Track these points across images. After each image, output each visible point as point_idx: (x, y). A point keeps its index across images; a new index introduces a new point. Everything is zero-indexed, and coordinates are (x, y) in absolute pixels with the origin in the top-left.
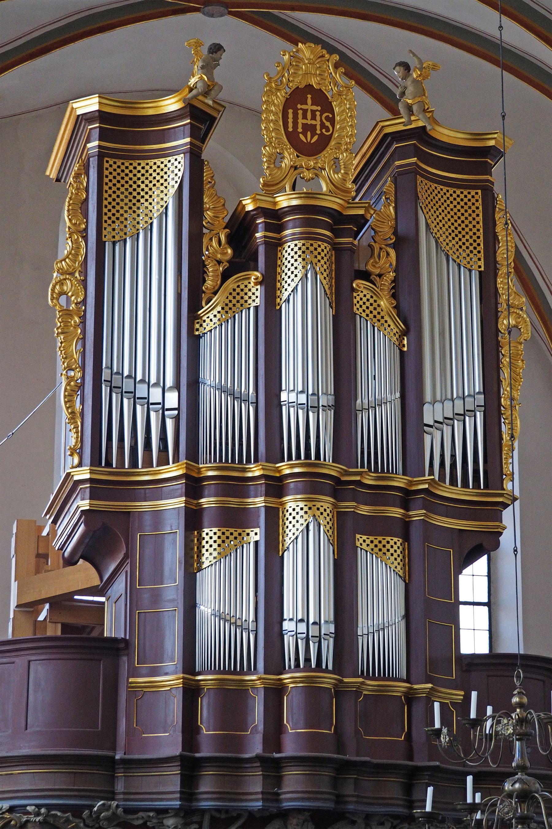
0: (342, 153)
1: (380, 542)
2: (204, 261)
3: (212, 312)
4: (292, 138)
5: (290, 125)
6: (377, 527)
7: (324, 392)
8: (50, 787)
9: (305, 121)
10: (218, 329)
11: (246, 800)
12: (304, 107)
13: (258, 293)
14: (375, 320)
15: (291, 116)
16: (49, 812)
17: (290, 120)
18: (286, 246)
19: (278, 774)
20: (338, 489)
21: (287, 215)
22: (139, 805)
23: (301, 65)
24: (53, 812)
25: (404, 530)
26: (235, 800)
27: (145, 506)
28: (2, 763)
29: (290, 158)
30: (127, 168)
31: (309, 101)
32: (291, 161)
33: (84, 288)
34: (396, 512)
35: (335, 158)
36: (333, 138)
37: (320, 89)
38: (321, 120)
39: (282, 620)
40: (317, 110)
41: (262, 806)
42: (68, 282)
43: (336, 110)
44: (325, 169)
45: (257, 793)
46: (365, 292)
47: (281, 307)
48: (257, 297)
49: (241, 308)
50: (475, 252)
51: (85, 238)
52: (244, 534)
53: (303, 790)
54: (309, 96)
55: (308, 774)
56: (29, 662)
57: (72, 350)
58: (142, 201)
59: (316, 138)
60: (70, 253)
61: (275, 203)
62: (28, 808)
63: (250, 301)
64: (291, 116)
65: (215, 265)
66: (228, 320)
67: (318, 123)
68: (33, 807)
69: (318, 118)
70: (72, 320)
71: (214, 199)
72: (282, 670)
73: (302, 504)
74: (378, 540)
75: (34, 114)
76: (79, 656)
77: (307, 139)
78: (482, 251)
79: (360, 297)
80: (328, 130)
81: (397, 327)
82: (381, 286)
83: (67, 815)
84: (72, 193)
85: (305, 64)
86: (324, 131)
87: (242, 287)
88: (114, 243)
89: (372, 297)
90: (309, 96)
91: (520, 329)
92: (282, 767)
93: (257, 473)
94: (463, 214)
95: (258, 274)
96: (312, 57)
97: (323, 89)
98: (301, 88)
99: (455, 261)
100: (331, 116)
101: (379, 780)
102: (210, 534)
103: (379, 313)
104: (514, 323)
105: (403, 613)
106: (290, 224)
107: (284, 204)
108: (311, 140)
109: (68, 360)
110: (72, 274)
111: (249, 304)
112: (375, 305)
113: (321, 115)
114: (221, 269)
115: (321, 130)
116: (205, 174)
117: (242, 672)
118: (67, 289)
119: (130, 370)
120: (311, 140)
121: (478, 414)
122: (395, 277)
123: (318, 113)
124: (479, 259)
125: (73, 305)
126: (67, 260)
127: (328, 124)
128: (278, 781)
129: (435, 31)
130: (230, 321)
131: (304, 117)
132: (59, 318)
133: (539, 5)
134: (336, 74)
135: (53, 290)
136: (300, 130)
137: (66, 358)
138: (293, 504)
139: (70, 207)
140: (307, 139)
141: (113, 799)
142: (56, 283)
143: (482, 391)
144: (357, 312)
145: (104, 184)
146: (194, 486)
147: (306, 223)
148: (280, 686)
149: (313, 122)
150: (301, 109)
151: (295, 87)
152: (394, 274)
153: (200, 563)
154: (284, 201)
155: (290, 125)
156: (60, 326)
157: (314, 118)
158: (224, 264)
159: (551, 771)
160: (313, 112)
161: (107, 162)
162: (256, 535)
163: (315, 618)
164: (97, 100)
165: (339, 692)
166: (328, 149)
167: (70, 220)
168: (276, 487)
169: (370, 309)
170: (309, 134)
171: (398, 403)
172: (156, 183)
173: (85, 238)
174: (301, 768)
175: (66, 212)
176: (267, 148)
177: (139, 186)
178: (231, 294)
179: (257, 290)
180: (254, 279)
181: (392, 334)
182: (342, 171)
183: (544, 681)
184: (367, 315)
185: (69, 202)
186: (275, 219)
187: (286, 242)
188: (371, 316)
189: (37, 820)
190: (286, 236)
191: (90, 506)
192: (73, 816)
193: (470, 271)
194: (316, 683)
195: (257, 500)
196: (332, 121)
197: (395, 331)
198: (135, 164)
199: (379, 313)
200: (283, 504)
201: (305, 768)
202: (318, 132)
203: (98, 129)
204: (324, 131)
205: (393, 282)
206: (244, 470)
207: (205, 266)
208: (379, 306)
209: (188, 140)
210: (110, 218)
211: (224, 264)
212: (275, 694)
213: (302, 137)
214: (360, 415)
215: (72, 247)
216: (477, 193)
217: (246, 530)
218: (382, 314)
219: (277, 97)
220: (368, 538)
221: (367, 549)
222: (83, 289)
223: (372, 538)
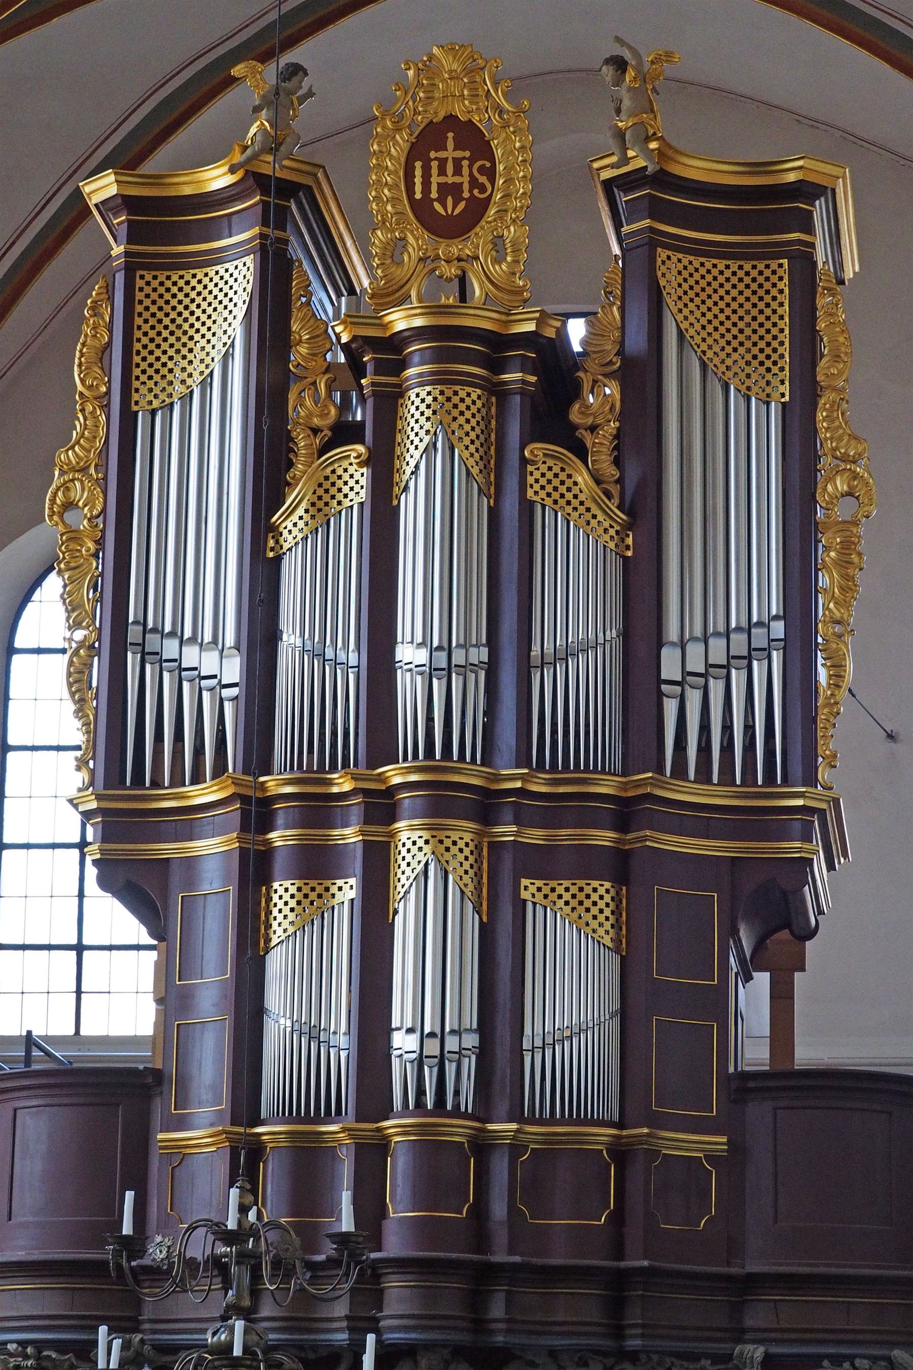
0: (508, 227)
1: (581, 889)
2: (290, 431)
3: (290, 520)
4: (422, 211)
5: (418, 188)
7: (462, 641)
8: (53, 1313)
9: (442, 179)
10: (300, 545)
11: (328, 1331)
12: (442, 154)
13: (363, 481)
14: (569, 509)
15: (418, 172)
16: (40, 1352)
17: (418, 180)
18: (412, 394)
19: (376, 1287)
20: (485, 806)
21: (409, 343)
22: (173, 1340)
23: (437, 81)
24: (45, 1353)
25: (620, 867)
26: (309, 1331)
27: (168, 849)
28: (2, 1272)
29: (418, 244)
30: (175, 284)
31: (450, 144)
32: (419, 250)
33: (102, 491)
34: (604, 837)
35: (495, 237)
36: (492, 201)
37: (470, 121)
38: (471, 175)
39: (388, 1031)
40: (464, 158)
41: (349, 1339)
42: (77, 484)
43: (499, 153)
44: (477, 258)
45: (339, 1319)
46: (550, 462)
47: (399, 502)
48: (362, 487)
49: (339, 508)
50: (775, 370)
51: (106, 408)
52: (334, 889)
53: (412, 1312)
54: (450, 135)
55: (422, 1287)
56: (15, 1110)
57: (83, 596)
58: (197, 337)
59: (462, 205)
60: (82, 436)
61: (385, 327)
62: (9, 1346)
63: (352, 495)
64: (418, 172)
65: (309, 436)
66: (317, 529)
67: (465, 180)
68: (15, 1346)
69: (465, 171)
70: (82, 546)
71: (309, 325)
72: (387, 1112)
74: (564, 886)
75: (336, 139)
76: (65, 1100)
77: (446, 211)
78: (787, 368)
79: (540, 472)
80: (483, 189)
81: (611, 518)
82: (593, 447)
83: (67, 1357)
84: (86, 336)
85: (443, 80)
86: (476, 192)
87: (340, 472)
88: (153, 413)
89: (563, 470)
90: (450, 135)
91: (857, 498)
92: (380, 1276)
93: (347, 787)
94: (734, 312)
95: (360, 448)
96: (455, 66)
97: (476, 119)
98: (437, 123)
99: (740, 391)
100: (488, 165)
101: (556, 1293)
102: (283, 890)
103: (575, 497)
104: (845, 488)
105: (617, 1006)
106: (416, 359)
107: (400, 326)
108: (453, 212)
109: (75, 614)
110: (84, 470)
111: (351, 500)
112: (569, 483)
113: (470, 167)
114: (318, 442)
115: (471, 191)
116: (294, 283)
117: (317, 1120)
118: (75, 497)
119: (174, 624)
120: (453, 212)
121: (775, 654)
122: (618, 429)
123: (465, 163)
124: (782, 382)
125: (85, 522)
126: (77, 448)
127: (483, 179)
128: (378, 1298)
129: (169, 120)
130: (320, 530)
131: (442, 172)
132: (63, 544)
133: (143, 102)
134: (496, 91)
135: (53, 501)
136: (434, 195)
137: (73, 610)
138: (410, 839)
139: (83, 359)
140: (446, 211)
141: (137, 1330)
142: (58, 489)
143: (781, 614)
144: (535, 498)
145: (136, 315)
146: (257, 814)
147: (439, 356)
148: (384, 1139)
149: (457, 179)
150: (436, 159)
151: (426, 121)
152: (617, 424)
153: (268, 940)
154: (400, 320)
155: (418, 188)
156: (64, 558)
157: (458, 171)
158: (323, 434)
159: (911, 1270)
160: (457, 163)
161: (142, 277)
162: (347, 890)
163: (432, 1025)
164: (112, 178)
165: (482, 1147)
166: (483, 223)
167: (82, 381)
168: (381, 807)
169: (560, 491)
170: (450, 201)
171: (618, 644)
172: (176, 316)
173: (106, 408)
174: (402, 1277)
175: (76, 368)
176: (379, 233)
177: (192, 313)
178: (320, 485)
179: (362, 475)
180: (355, 458)
181: (600, 531)
182: (509, 259)
183: (890, 1114)
184: (555, 502)
185: (81, 351)
186: (392, 350)
187: (409, 389)
188: (562, 502)
189: (29, 1364)
190: (407, 379)
191: (101, 854)
192: (78, 1357)
193: (768, 404)
194: (444, 1135)
195: (347, 831)
196: (491, 174)
197: (606, 524)
198: (175, 278)
199: (575, 497)
200: (393, 835)
201: (409, 1277)
202: (466, 195)
203: (126, 224)
204: (476, 192)
205: (617, 437)
206: (330, 783)
207: (292, 440)
208: (576, 484)
209: (256, 230)
210: (144, 372)
211: (323, 434)
212: (373, 1154)
213: (437, 206)
214: (539, 674)
215: (86, 425)
216: (781, 266)
217: (337, 881)
218: (582, 497)
219: (396, 143)
220: (534, 884)
221: (544, 902)
222: (101, 495)
223: (539, 883)
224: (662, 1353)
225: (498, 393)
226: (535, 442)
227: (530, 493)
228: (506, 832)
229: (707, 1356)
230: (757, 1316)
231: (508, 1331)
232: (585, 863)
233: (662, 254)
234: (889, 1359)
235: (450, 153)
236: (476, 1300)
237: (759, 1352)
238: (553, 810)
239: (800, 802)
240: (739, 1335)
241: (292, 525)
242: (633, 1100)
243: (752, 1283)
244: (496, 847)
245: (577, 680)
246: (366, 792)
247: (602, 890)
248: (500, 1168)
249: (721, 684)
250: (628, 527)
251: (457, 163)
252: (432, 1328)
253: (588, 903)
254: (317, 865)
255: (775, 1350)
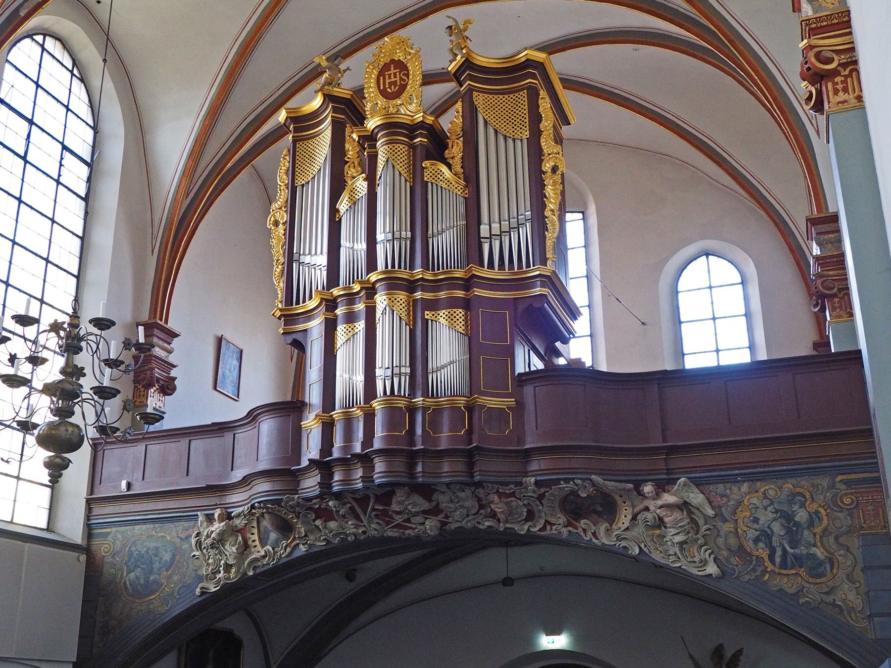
6: (433, 305)
20: (411, 286)
25: (466, 304)
31: (392, 68)
34: (460, 294)
67: (398, 78)
73: (385, 297)
102: (341, 329)
117: (437, 397)
127: (404, 77)
131: (390, 78)
138: (381, 300)
146: (331, 304)
157: (395, 77)
160: (395, 74)
162: (361, 325)
168: (370, 291)
196: (408, 75)
212: (369, 417)
224: (491, 482)
225: (413, 147)
226: (656, 282)
227: (426, 179)
228: (418, 295)
229: (512, 483)
230: (534, 466)
231: (423, 476)
232: (452, 303)
233: (475, 94)
234: (590, 480)
235: (392, 71)
236: (412, 466)
237: (533, 480)
238: (435, 286)
239: (538, 273)
240: (526, 474)
241: (343, 206)
242: (473, 386)
243: (528, 454)
244: (415, 301)
245: (446, 240)
246: (366, 288)
247: (460, 313)
248: (419, 418)
249: (507, 238)
250: (466, 186)
251: (395, 74)
252: (390, 476)
253: (455, 320)
254: (351, 318)
255: (539, 478)
